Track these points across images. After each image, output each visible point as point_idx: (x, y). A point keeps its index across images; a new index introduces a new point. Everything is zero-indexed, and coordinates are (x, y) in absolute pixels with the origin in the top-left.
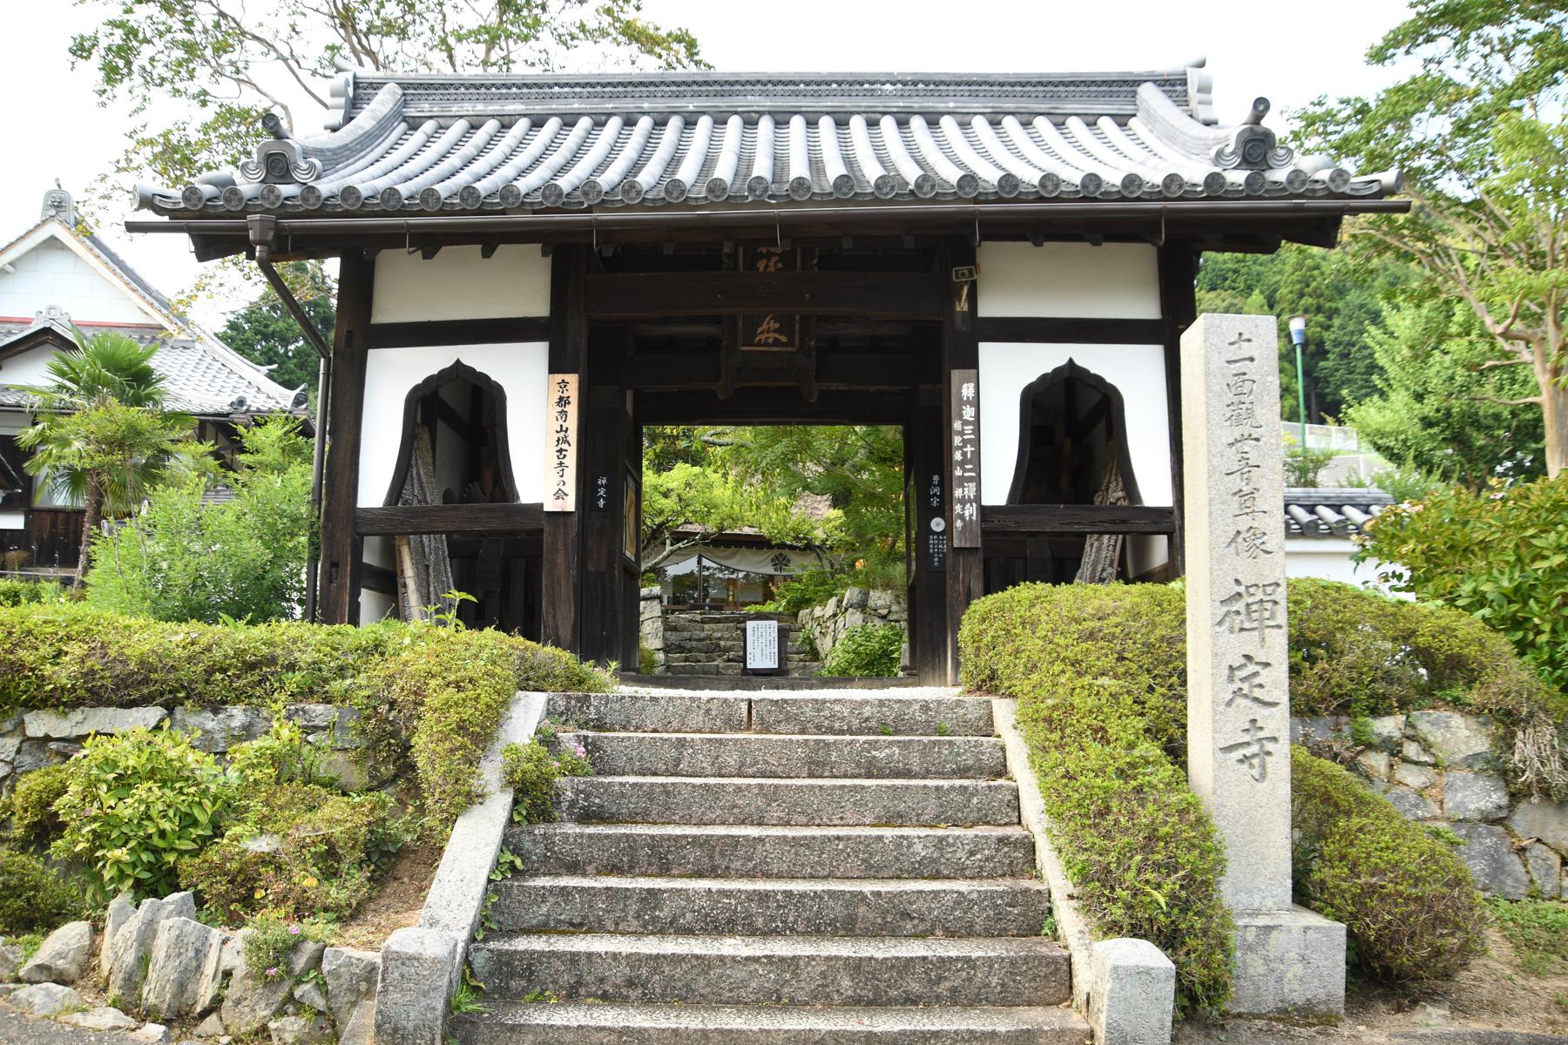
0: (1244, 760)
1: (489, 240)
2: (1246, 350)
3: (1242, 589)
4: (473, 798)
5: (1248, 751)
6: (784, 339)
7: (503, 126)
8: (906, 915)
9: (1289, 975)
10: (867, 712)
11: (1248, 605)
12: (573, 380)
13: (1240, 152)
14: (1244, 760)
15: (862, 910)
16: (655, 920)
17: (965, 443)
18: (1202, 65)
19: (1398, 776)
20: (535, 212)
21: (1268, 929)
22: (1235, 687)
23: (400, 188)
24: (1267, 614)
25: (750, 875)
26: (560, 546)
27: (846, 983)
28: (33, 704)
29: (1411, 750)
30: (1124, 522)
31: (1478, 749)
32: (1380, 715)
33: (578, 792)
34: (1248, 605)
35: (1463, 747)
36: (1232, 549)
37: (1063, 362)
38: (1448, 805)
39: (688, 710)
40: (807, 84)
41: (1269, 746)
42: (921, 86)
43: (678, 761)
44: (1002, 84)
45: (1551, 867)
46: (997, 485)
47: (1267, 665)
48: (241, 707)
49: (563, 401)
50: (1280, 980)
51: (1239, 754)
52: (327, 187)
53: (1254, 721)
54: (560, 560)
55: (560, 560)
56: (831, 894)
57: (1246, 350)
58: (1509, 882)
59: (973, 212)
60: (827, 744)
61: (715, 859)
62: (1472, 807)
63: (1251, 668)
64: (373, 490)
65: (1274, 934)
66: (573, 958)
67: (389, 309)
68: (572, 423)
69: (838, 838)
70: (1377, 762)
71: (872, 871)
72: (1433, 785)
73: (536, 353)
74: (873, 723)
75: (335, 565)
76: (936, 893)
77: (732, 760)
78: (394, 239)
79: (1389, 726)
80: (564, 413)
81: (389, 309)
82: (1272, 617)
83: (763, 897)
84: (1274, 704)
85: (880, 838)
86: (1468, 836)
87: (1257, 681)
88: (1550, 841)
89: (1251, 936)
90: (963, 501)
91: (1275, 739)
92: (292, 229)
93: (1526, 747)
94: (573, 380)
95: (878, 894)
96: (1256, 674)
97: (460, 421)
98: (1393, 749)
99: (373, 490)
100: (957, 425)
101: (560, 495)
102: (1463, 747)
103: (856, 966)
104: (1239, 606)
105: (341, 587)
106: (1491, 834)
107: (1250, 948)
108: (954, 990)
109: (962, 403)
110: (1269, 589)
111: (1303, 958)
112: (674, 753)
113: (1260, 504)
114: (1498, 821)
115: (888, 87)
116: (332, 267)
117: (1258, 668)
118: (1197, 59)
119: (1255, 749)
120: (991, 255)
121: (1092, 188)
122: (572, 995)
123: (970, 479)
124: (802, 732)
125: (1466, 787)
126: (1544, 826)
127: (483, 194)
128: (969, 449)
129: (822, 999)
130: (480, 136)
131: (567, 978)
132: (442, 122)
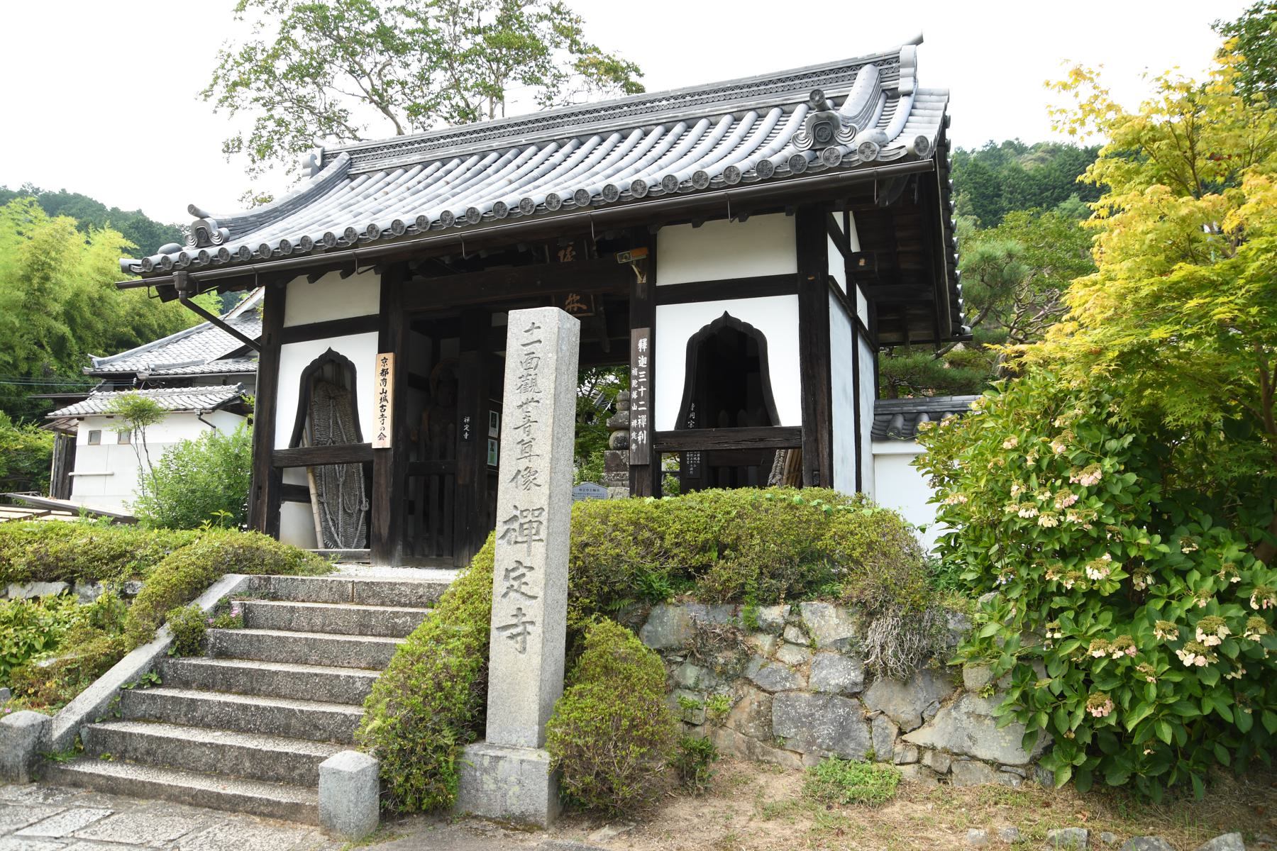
0: (512, 637)
1: (347, 267)
2: (537, 334)
3: (518, 513)
4: (144, 638)
5: (514, 631)
6: (584, 307)
7: (784, 112)
8: (316, 727)
9: (511, 793)
10: (421, 591)
11: (522, 525)
12: (390, 356)
13: (811, 136)
14: (512, 637)
15: (293, 721)
16: (193, 717)
17: (639, 384)
18: (919, 41)
19: (778, 655)
20: (327, 251)
21: (498, 758)
22: (508, 584)
23: (504, 200)
24: (534, 531)
25: (268, 695)
26: (383, 471)
27: (247, 764)
28: (11, 579)
29: (791, 633)
30: (761, 440)
31: (844, 635)
32: (769, 605)
33: (216, 638)
34: (522, 525)
35: (833, 633)
36: (513, 484)
37: (720, 315)
38: (813, 680)
39: (321, 588)
40: (606, 110)
41: (529, 628)
42: (688, 98)
43: (291, 621)
44: (749, 86)
45: (888, 736)
46: (667, 419)
47: (531, 568)
48: (105, 582)
49: (384, 372)
50: (504, 796)
51: (508, 633)
52: (232, 247)
53: (520, 609)
54: (383, 481)
55: (383, 481)
56: (279, 709)
57: (537, 334)
58: (852, 745)
59: (871, 175)
60: (370, 613)
61: (254, 684)
62: (833, 682)
63: (522, 570)
64: (282, 441)
65: (501, 762)
66: (124, 735)
67: (296, 317)
68: (389, 388)
69: (316, 675)
70: (763, 642)
71: (333, 699)
72: (806, 663)
73: (372, 338)
74: (424, 599)
75: (260, 488)
76: (332, 714)
77: (318, 621)
78: (289, 274)
79: (774, 614)
80: (384, 380)
81: (296, 317)
82: (537, 533)
83: (245, 708)
84: (535, 598)
85: (338, 676)
86: (825, 706)
87: (524, 580)
88: (891, 714)
89: (486, 762)
90: (637, 430)
91: (532, 623)
92: (198, 278)
93: (875, 636)
94: (390, 356)
95: (302, 711)
96: (524, 575)
97: (331, 382)
98: (776, 631)
99: (282, 441)
100: (634, 372)
101: (382, 437)
102: (833, 633)
103: (253, 754)
104: (516, 525)
105: (262, 503)
106: (845, 705)
107: (485, 771)
108: (301, 776)
109: (638, 354)
110: (536, 513)
111: (519, 782)
112: (289, 616)
113: (536, 450)
114: (854, 695)
115: (664, 102)
116: (260, 294)
117: (524, 571)
118: (915, 36)
119: (519, 629)
120: (670, 237)
121: (671, 186)
122: (121, 758)
123: (642, 413)
124: (383, 604)
125: (832, 664)
126: (889, 700)
127: (620, 190)
128: (642, 389)
129: (236, 774)
130: (717, 131)
131: (121, 748)
132: (713, 119)
